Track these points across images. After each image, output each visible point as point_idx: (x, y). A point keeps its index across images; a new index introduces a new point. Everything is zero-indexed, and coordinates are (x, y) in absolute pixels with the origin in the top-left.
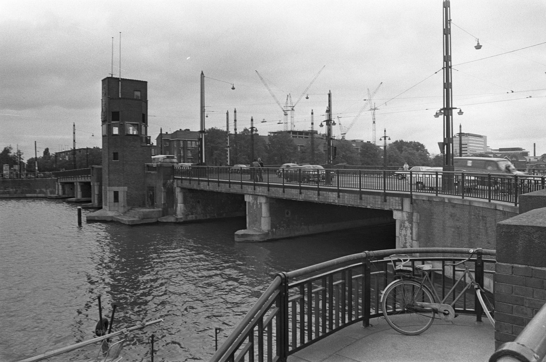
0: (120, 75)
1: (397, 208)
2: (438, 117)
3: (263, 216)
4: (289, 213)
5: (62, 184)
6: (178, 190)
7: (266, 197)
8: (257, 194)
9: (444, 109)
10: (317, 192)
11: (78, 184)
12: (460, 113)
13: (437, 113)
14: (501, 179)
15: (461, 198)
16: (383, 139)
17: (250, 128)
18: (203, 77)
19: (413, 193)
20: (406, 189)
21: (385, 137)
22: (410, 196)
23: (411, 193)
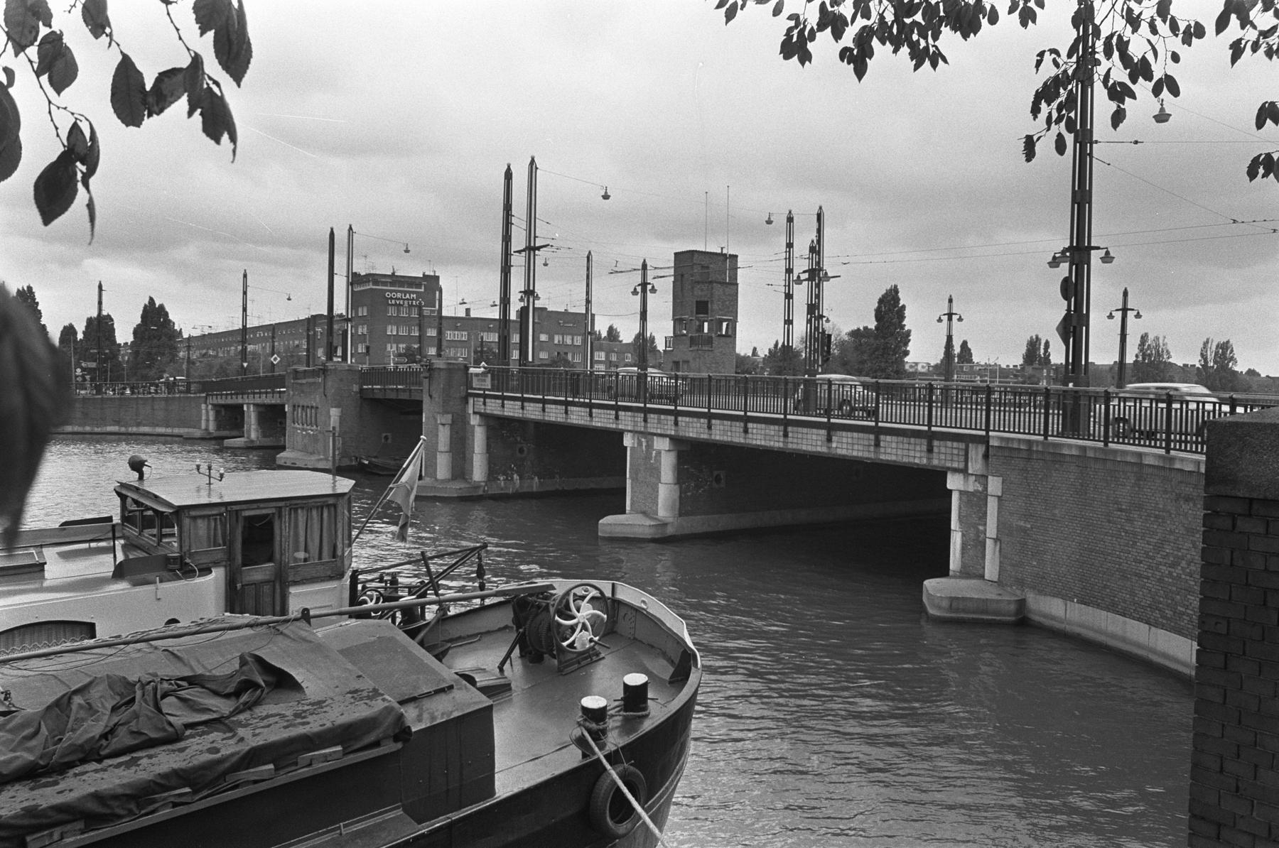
0: (668, 268)
1: (955, 465)
2: (1058, 266)
3: (662, 481)
4: (720, 479)
5: (218, 409)
6: (474, 420)
7: (672, 438)
8: (652, 431)
9: (1070, 249)
10: (519, 403)
11: (252, 408)
12: (1106, 260)
13: (1054, 258)
14: (1198, 403)
15: (1162, 452)
16: (945, 318)
17: (639, 285)
18: (534, 170)
19: (991, 433)
20: (1024, 429)
21: (950, 315)
22: (985, 440)
23: (987, 433)
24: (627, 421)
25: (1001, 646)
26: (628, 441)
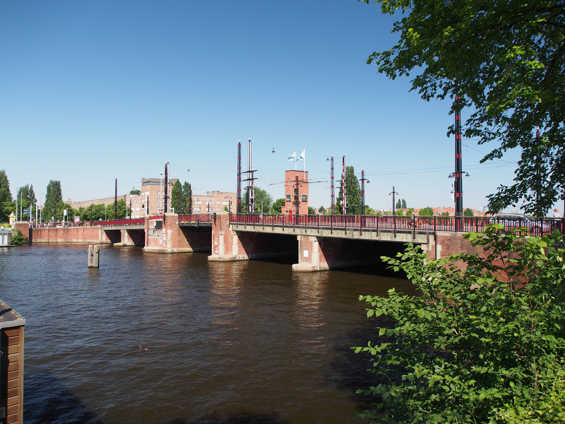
7: (317, 237)
24: (298, 232)
25: (117, 318)
26: (299, 238)
